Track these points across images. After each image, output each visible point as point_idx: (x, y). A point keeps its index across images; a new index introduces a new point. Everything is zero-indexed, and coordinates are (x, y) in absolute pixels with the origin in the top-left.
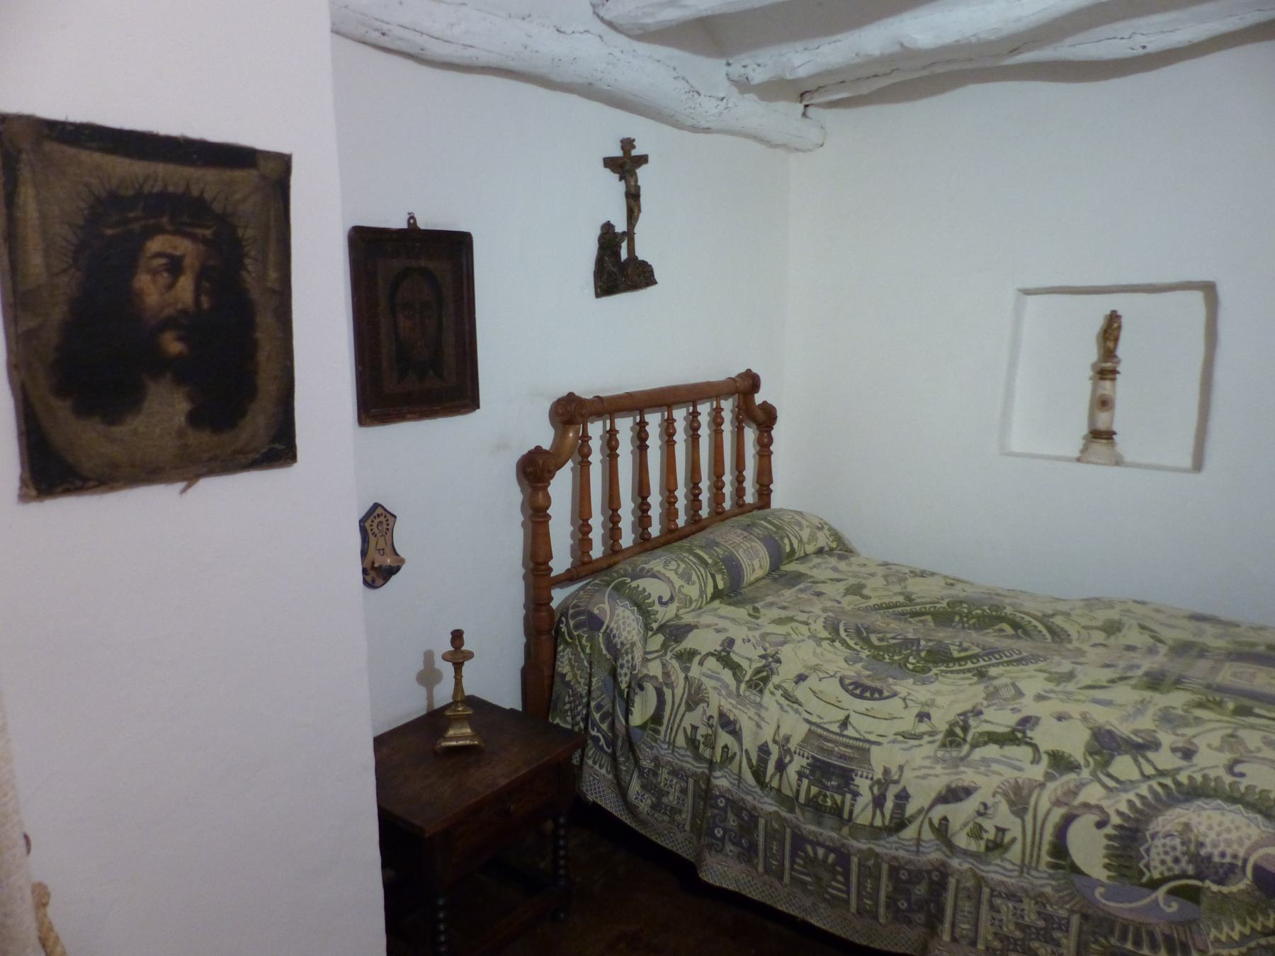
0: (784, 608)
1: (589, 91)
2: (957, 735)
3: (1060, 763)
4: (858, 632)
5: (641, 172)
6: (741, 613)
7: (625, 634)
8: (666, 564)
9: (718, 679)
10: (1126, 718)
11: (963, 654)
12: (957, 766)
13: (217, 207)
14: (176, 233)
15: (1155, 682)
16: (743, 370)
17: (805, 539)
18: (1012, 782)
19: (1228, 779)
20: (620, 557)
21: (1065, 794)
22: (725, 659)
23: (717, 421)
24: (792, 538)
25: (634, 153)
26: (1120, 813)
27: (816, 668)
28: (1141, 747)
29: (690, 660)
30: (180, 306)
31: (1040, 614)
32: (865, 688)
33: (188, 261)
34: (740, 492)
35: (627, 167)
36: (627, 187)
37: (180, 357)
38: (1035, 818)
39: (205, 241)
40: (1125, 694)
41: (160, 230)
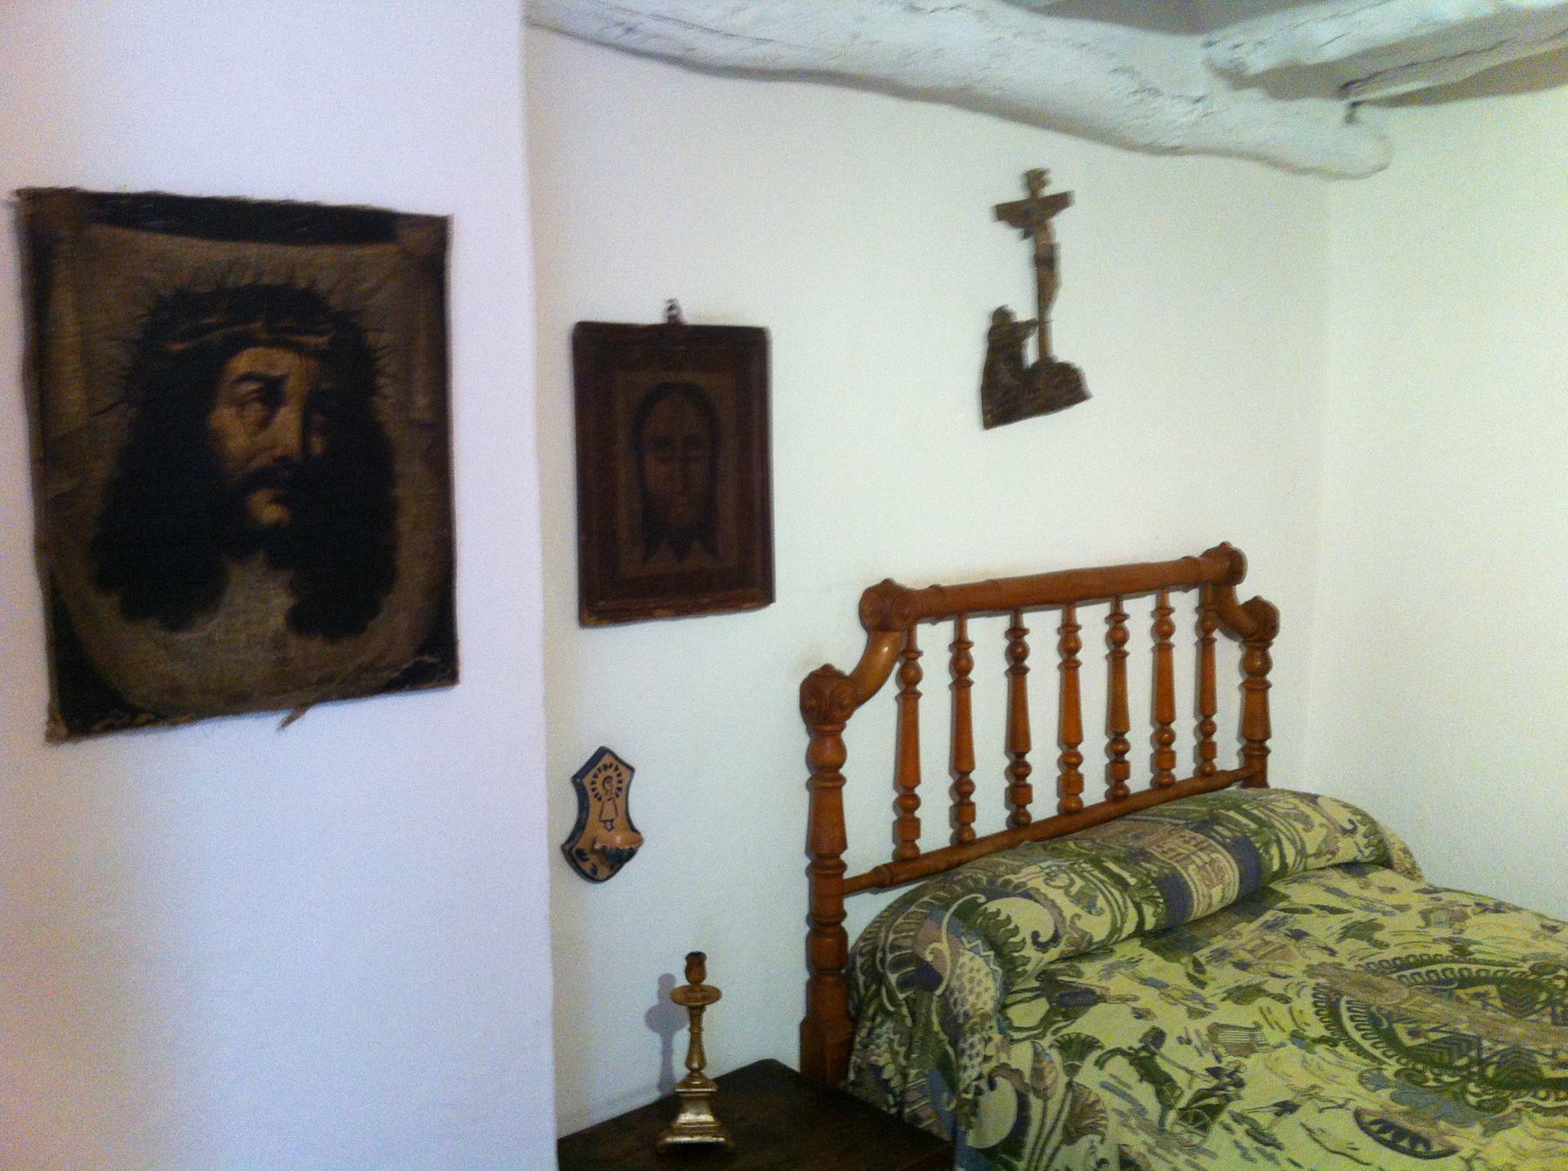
0: (1242, 966)
1: (966, 98)
6: (1174, 973)
7: (971, 999)
8: (1050, 878)
9: (1123, 1095)
13: (336, 302)
14: (272, 344)
16: (1214, 543)
17: (1311, 850)
20: (971, 852)
23: (1163, 629)
24: (1286, 844)
25: (1048, 191)
27: (1311, 1093)
29: (1082, 1057)
30: (278, 452)
32: (1401, 1133)
33: (292, 385)
34: (1206, 749)
37: (276, 527)
39: (318, 354)
41: (250, 341)
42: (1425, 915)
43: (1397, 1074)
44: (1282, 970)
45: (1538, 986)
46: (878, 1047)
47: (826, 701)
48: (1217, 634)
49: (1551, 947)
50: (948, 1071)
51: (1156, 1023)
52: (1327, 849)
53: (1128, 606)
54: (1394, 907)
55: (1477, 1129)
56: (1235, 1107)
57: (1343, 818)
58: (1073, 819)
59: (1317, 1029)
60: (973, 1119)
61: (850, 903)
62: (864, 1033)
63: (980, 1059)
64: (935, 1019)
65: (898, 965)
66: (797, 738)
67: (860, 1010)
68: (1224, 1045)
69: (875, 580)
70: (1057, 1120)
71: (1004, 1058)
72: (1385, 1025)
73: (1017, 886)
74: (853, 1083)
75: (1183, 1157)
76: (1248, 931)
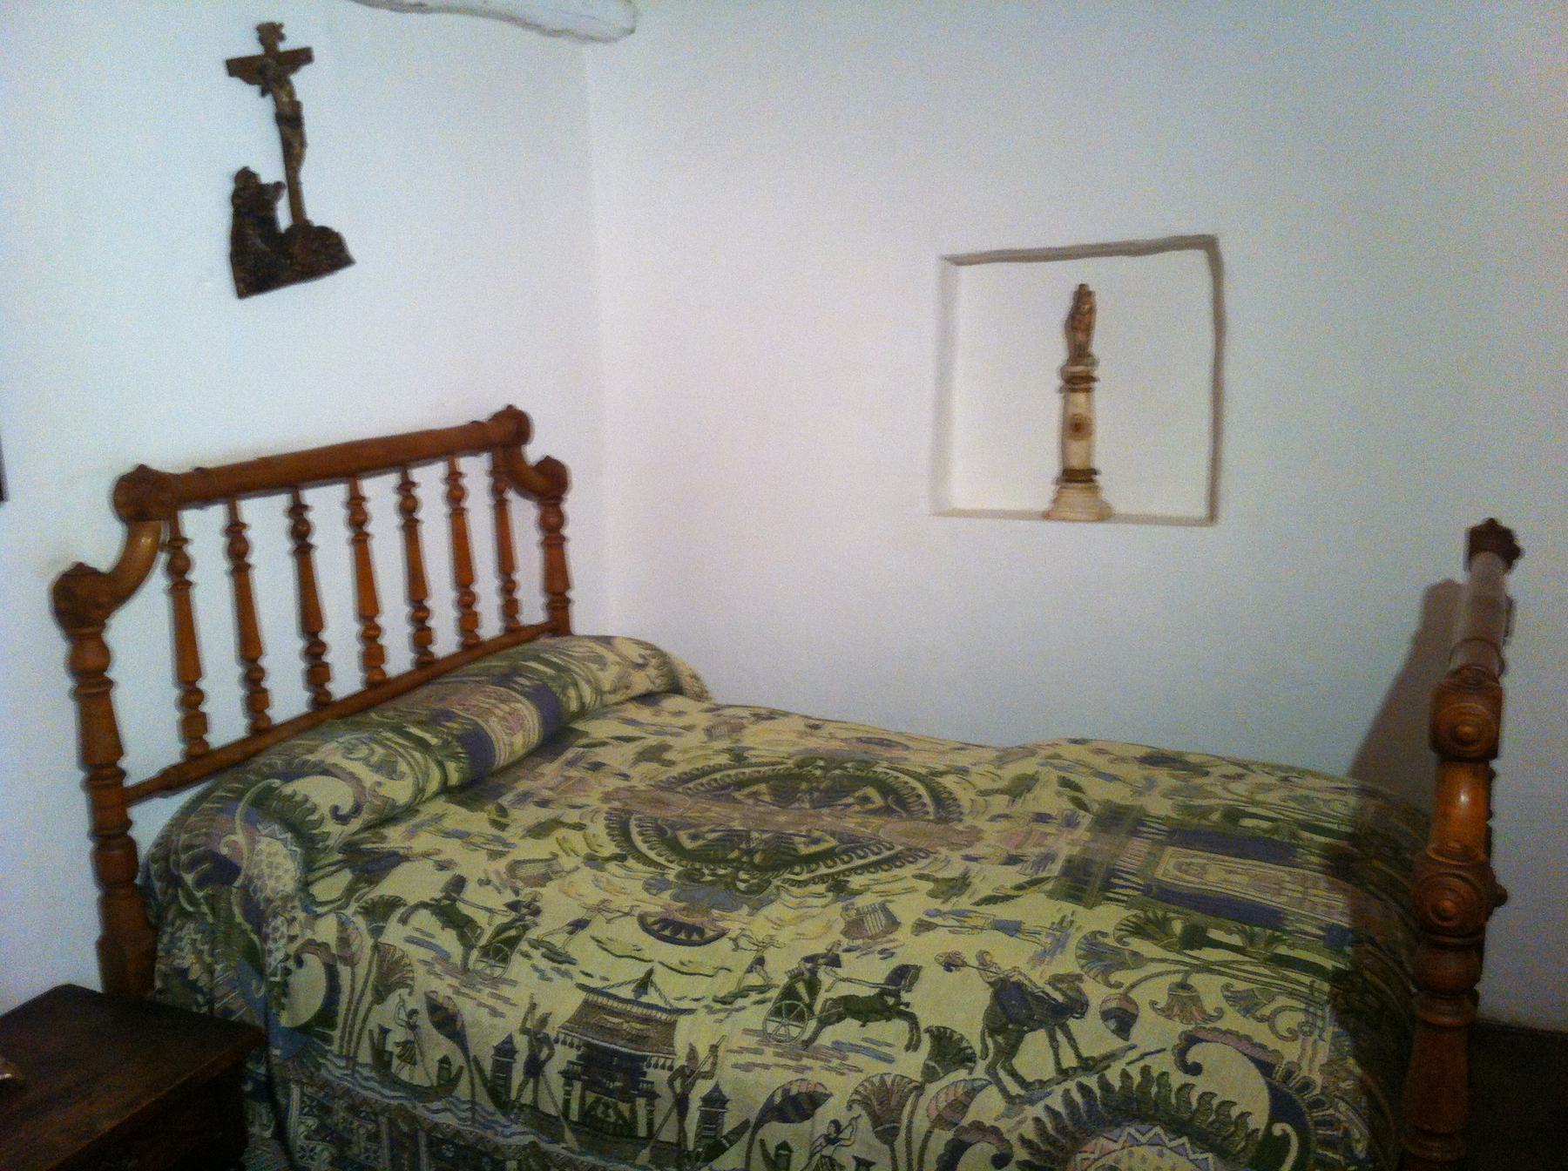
0: (544, 803)
2: (800, 999)
3: (948, 1050)
4: (660, 832)
5: (302, 81)
6: (477, 821)
7: (271, 883)
10: (1039, 959)
11: (814, 849)
12: (799, 1058)
15: (1081, 882)
16: (499, 406)
17: (607, 687)
18: (876, 1080)
19: (1177, 1079)
20: (268, 739)
21: (950, 1105)
22: (448, 911)
23: (455, 494)
25: (283, 47)
26: (1025, 1142)
28: (1058, 1012)
29: (386, 918)
31: (924, 771)
32: (679, 927)
34: (510, 607)
35: (270, 73)
36: (277, 100)
38: (909, 1143)
40: (1039, 910)
42: (709, 731)
43: (678, 876)
44: (579, 801)
45: (802, 778)
46: (181, 949)
47: (83, 602)
48: (511, 495)
49: (812, 743)
50: (255, 959)
51: (458, 871)
52: (622, 684)
53: (417, 474)
54: (684, 728)
55: (745, 910)
56: (533, 934)
57: (634, 653)
58: (380, 690)
59: (610, 849)
60: (284, 1000)
61: (137, 813)
62: (165, 939)
63: (284, 941)
64: (237, 910)
65: (192, 865)
66: (53, 645)
67: (160, 917)
68: (522, 879)
69: (127, 467)
70: (366, 982)
71: (309, 935)
72: (669, 832)
73: (315, 765)
74: (160, 992)
75: (487, 990)
76: (551, 771)
